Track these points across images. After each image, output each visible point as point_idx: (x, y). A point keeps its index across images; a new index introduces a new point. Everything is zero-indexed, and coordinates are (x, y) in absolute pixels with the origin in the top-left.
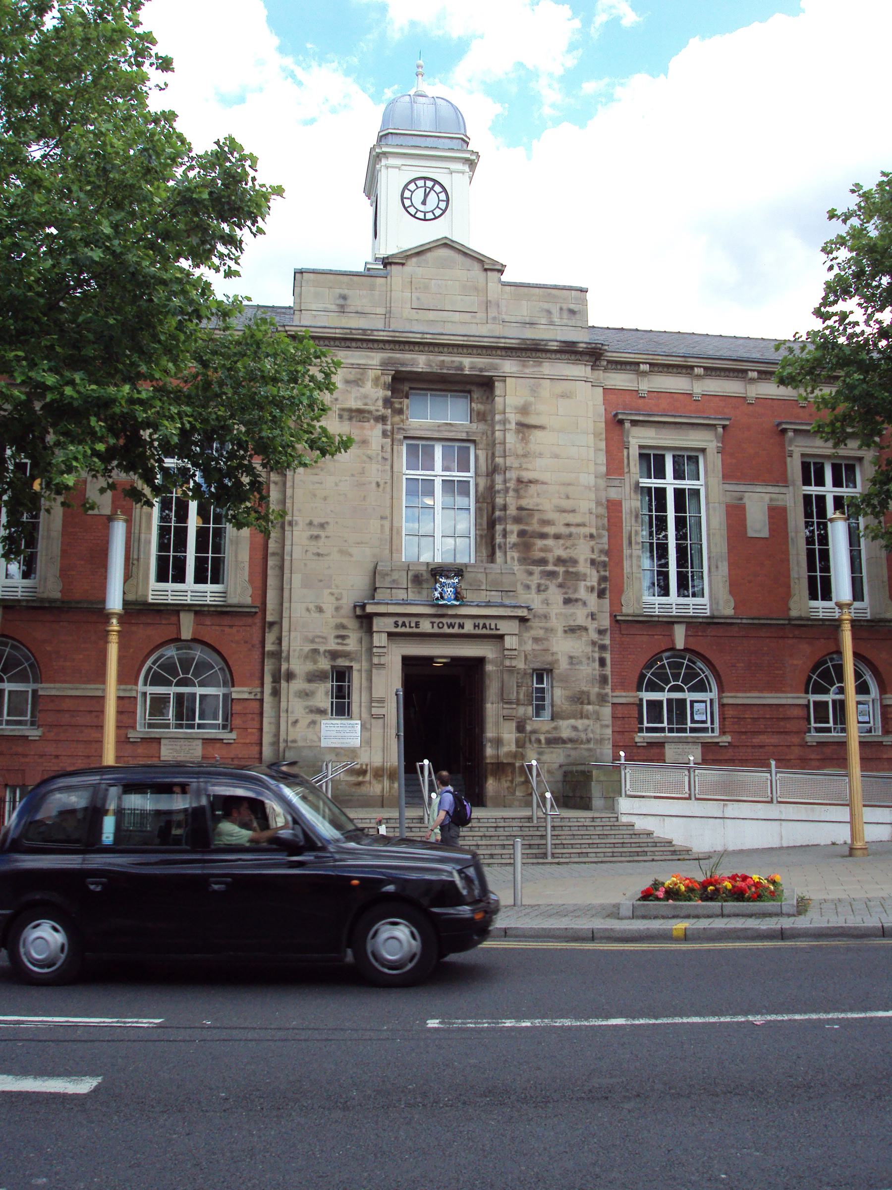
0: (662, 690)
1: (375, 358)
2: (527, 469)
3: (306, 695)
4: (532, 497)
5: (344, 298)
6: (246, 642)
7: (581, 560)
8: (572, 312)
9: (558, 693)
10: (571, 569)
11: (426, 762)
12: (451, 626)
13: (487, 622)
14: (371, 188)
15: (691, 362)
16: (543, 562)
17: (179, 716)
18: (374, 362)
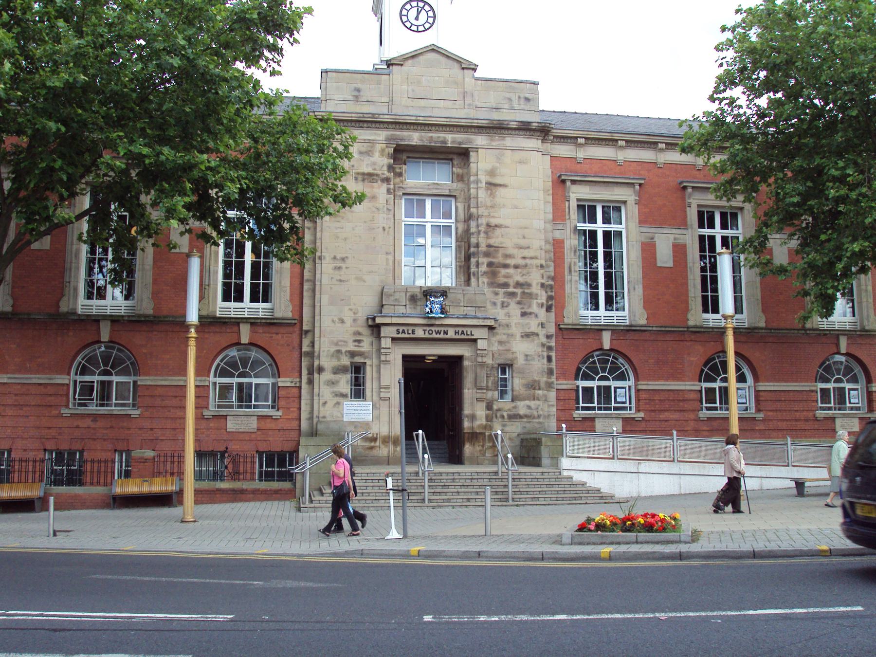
0: (594, 379)
1: (381, 135)
2: (493, 217)
3: (333, 383)
5: (358, 90)
7: (534, 284)
9: (517, 381)
10: (526, 291)
12: (438, 332)
13: (465, 330)
17: (240, 399)
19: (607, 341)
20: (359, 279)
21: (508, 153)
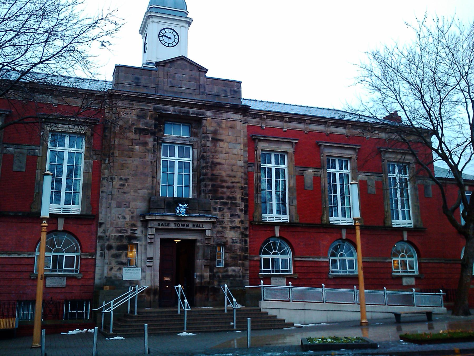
0: (270, 254)
4: (218, 170)
5: (138, 79)
6: (89, 232)
7: (238, 197)
8: (235, 92)
10: (233, 202)
11: (180, 286)
14: (143, 30)
16: (222, 198)
18: (151, 108)
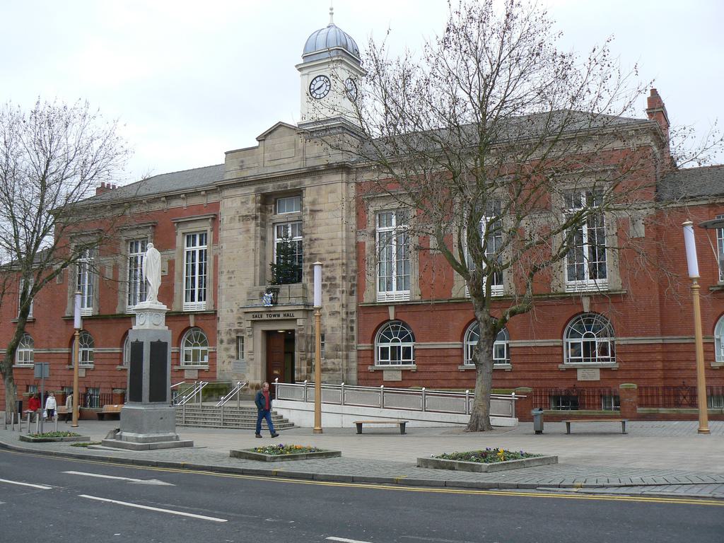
0: (389, 341)
1: (252, 189)
2: (314, 233)
3: (227, 349)
7: (338, 277)
10: (333, 283)
12: (274, 316)
13: (289, 313)
15: (199, 189)
17: (586, 354)
19: (586, 304)
20: (240, 284)
21: (324, 187)
